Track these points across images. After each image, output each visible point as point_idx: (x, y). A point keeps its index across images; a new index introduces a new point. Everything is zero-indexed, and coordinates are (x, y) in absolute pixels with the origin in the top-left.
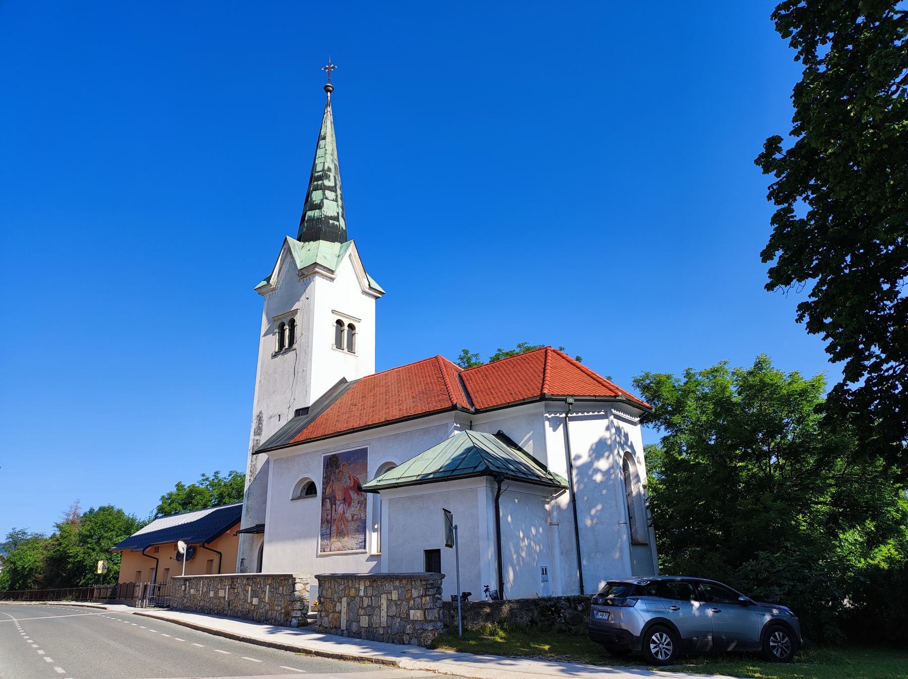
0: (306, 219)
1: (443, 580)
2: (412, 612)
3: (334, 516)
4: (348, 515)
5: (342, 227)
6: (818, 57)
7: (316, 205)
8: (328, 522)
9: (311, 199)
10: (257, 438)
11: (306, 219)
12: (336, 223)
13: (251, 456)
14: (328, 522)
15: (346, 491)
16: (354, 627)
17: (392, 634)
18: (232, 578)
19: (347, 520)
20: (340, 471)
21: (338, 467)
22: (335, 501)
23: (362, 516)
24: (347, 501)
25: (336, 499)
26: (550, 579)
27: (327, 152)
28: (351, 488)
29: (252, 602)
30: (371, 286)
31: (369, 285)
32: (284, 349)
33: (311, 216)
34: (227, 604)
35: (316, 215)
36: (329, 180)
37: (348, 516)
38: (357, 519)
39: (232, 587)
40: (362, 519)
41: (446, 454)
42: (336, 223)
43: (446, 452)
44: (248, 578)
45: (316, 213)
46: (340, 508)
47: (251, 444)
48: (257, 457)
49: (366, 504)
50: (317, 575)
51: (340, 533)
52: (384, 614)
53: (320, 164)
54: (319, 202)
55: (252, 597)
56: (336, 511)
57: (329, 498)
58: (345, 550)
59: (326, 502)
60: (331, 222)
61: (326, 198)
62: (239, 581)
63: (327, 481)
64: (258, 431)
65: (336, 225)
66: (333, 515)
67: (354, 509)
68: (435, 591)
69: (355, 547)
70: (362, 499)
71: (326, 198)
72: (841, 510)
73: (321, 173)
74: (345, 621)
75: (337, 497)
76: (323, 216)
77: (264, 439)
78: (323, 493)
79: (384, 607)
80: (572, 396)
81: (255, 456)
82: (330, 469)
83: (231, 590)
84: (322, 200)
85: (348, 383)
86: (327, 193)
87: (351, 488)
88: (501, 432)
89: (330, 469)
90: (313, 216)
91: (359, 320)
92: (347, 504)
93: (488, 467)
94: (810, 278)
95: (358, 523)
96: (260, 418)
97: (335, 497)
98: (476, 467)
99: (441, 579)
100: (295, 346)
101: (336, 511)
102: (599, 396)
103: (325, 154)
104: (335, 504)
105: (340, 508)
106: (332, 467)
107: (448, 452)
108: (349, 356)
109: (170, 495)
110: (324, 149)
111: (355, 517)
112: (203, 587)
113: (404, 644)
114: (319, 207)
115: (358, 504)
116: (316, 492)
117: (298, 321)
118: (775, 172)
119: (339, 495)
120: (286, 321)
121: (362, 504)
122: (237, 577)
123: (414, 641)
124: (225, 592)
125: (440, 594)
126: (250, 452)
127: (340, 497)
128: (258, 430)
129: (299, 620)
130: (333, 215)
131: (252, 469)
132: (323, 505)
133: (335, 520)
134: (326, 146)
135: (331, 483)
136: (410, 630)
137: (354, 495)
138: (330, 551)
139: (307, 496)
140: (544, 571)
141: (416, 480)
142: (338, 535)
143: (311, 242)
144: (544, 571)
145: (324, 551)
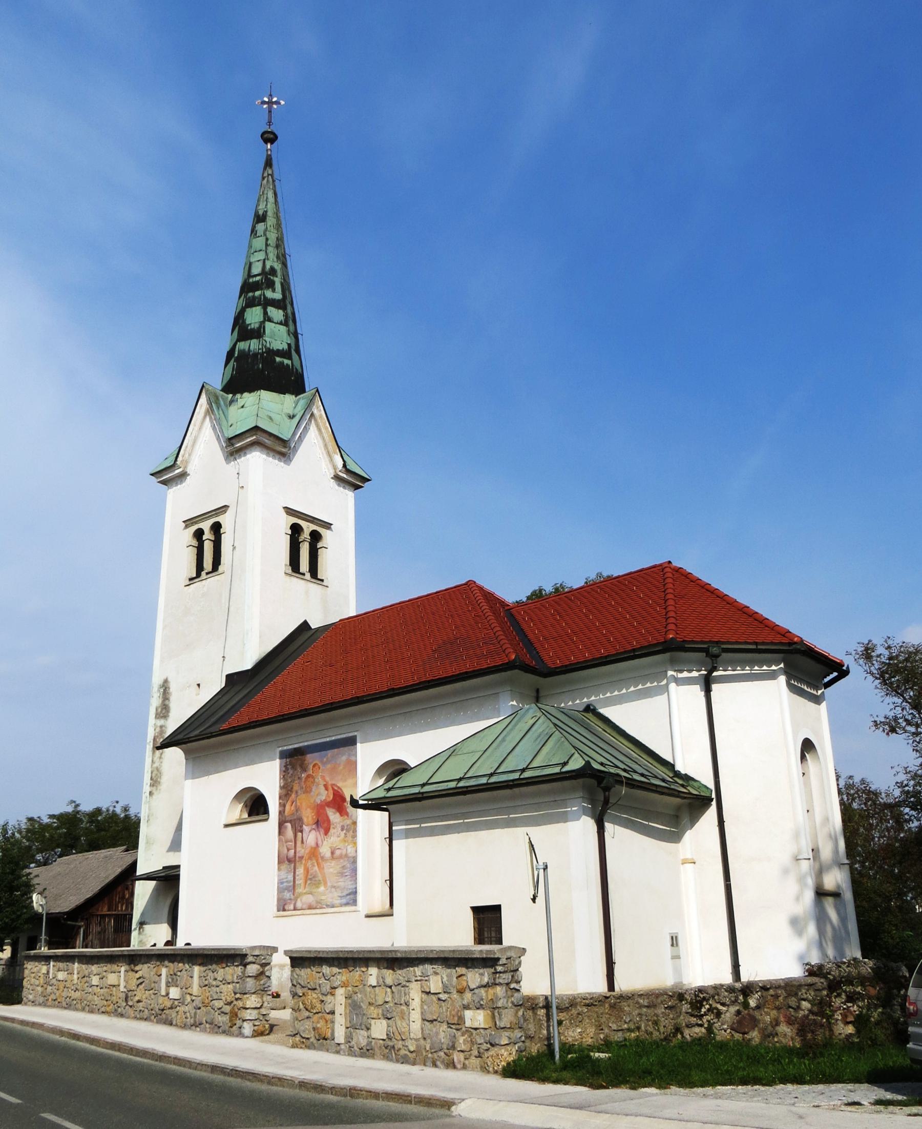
0: (236, 355)
1: (522, 958)
2: (468, 1014)
3: (301, 851)
4: (325, 850)
5: (296, 369)
7: (253, 330)
8: (289, 861)
9: (244, 321)
10: (161, 722)
11: (236, 355)
12: (286, 361)
13: (151, 753)
14: (289, 861)
15: (320, 809)
16: (361, 1038)
17: (433, 1051)
19: (322, 858)
20: (308, 776)
21: (304, 770)
22: (301, 827)
23: (349, 850)
24: (323, 825)
25: (303, 823)
26: (682, 953)
27: (269, 242)
28: (329, 804)
30: (348, 467)
31: (345, 466)
32: (203, 573)
33: (244, 350)
35: (252, 348)
36: (274, 291)
37: (325, 850)
38: (341, 857)
40: (350, 855)
41: (505, 743)
42: (286, 361)
43: (503, 740)
45: (253, 345)
46: (311, 837)
47: (151, 733)
48: (161, 754)
49: (355, 831)
50: (288, 951)
51: (311, 879)
52: (416, 1016)
53: (257, 263)
54: (257, 326)
55: (168, 985)
56: (302, 842)
57: (290, 822)
58: (321, 908)
59: (286, 827)
60: (278, 359)
61: (270, 320)
63: (286, 792)
64: (164, 711)
65: (287, 364)
66: (298, 849)
67: (334, 839)
68: (510, 977)
69: (337, 902)
70: (349, 822)
71: (270, 320)
73: (258, 278)
75: (305, 820)
76: (264, 350)
77: (172, 724)
78: (280, 812)
79: (416, 1003)
80: (717, 642)
81: (158, 752)
82: (291, 771)
84: (262, 324)
85: (311, 633)
86: (272, 311)
87: (329, 804)
88: (592, 707)
89: (291, 771)
90: (247, 350)
91: (328, 526)
92: (322, 831)
93: (588, 763)
95: (343, 862)
96: (165, 687)
97: (300, 820)
98: (565, 764)
99: (520, 957)
100: (221, 568)
101: (302, 842)
102: (763, 643)
103: (267, 245)
104: (301, 831)
105: (311, 837)
106: (294, 768)
107: (508, 739)
108: (314, 587)
110: (263, 239)
111: (338, 853)
113: (455, 1067)
114: (258, 333)
115: (342, 830)
116: (266, 811)
117: (227, 528)
118: (125, 847)
119: (308, 816)
120: (206, 526)
121: (348, 830)
123: (474, 1061)
125: (518, 982)
126: (150, 747)
127: (310, 819)
128: (162, 709)
129: (255, 1026)
130: (281, 348)
131: (154, 775)
132: (280, 833)
133: (301, 858)
134: (268, 233)
135: (293, 796)
136: (465, 1044)
137: (333, 816)
138: (295, 909)
139: (253, 818)
140: (674, 941)
141: (456, 788)
142: (309, 882)
143: (246, 394)
144: (674, 941)
145: (284, 910)
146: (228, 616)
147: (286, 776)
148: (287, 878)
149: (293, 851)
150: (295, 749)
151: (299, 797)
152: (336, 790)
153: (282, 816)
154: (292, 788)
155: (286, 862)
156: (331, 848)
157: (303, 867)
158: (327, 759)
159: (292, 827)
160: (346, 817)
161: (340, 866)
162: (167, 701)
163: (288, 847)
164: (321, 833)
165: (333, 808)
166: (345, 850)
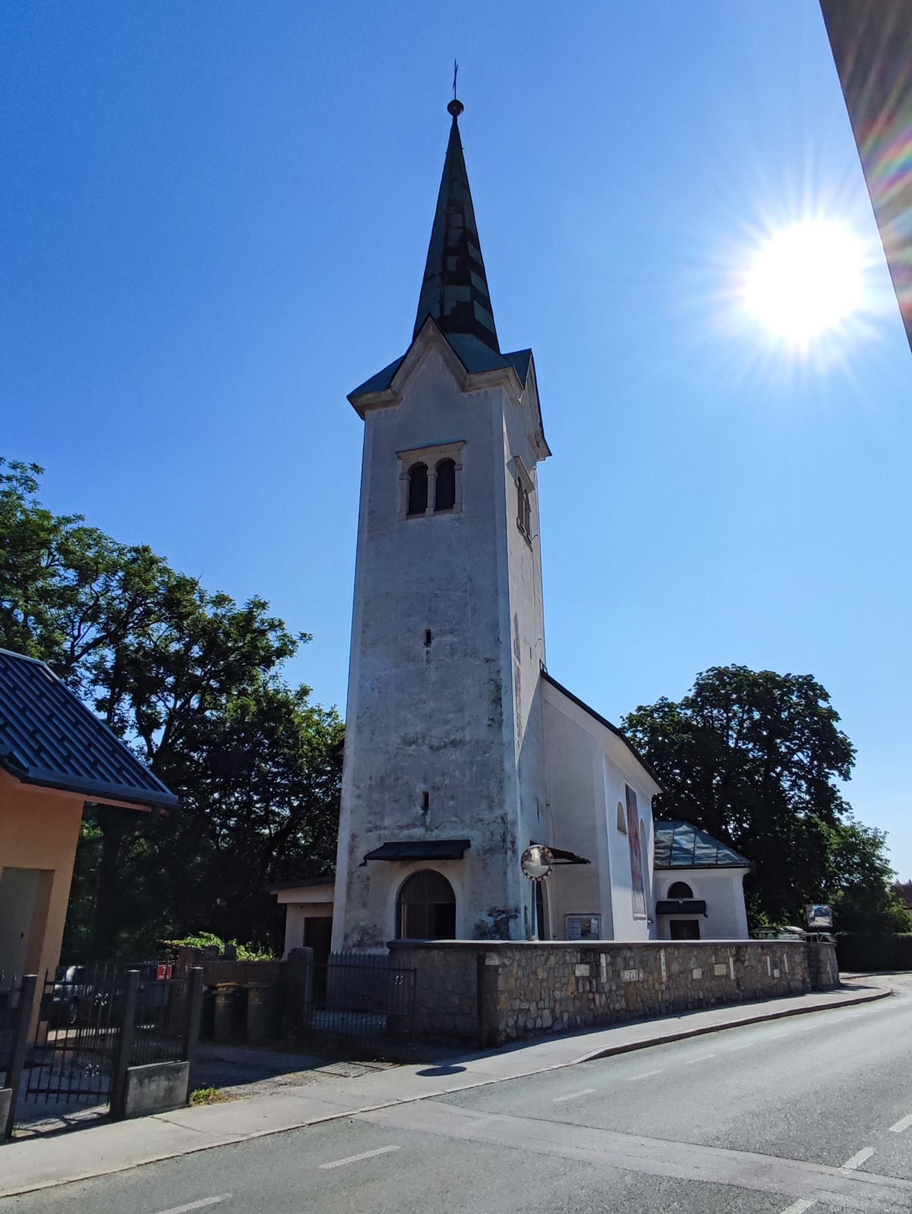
6: (846, 776)
18: (739, 946)
29: (773, 975)
34: (735, 985)
39: (738, 959)
44: (763, 946)
55: (772, 970)
62: (749, 950)
72: (322, 868)
74: (371, 1152)
83: (738, 964)
94: (476, 318)
109: (665, 708)
112: (223, 987)
122: (746, 945)
124: (728, 967)
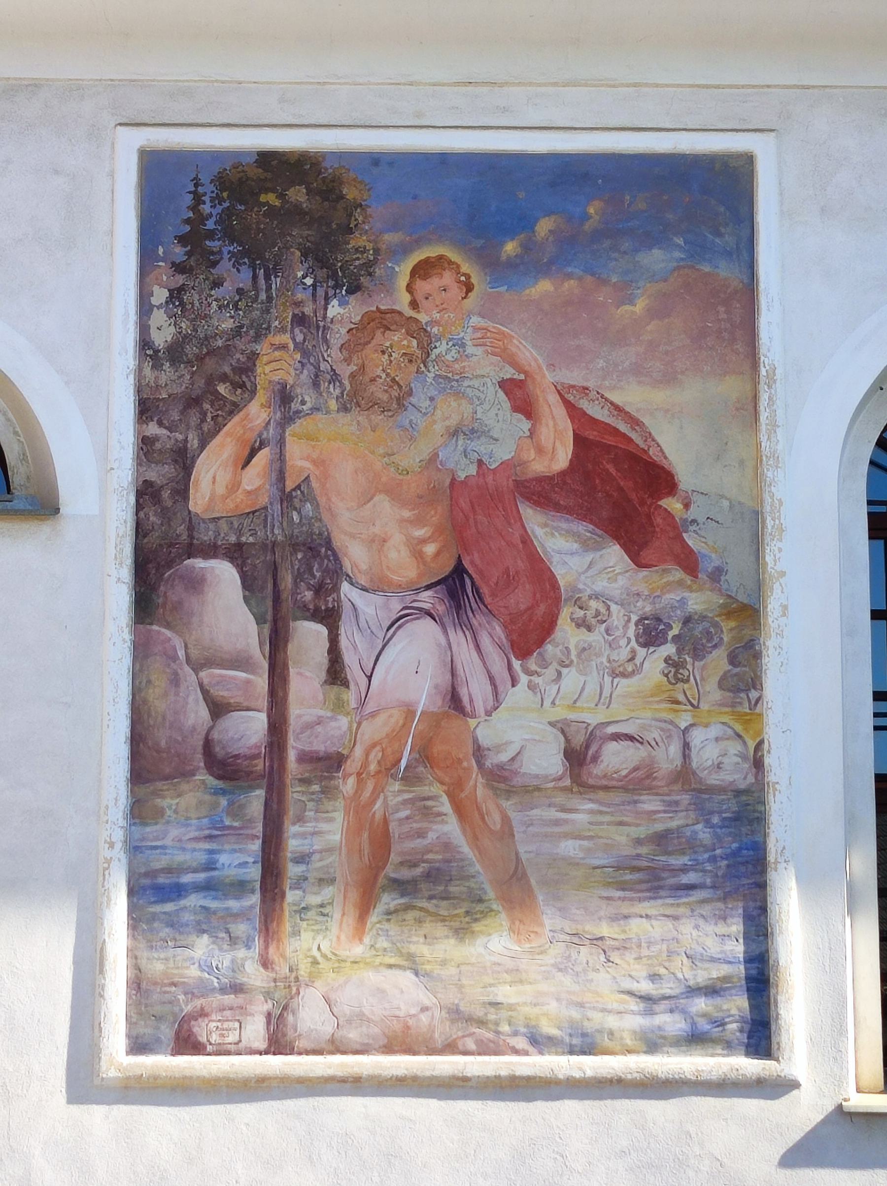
146: (375, 664)
147: (192, 297)
148: (210, 866)
149: (261, 719)
150: (266, 158)
151: (297, 427)
152: (594, 422)
153: (166, 515)
154: (248, 367)
155: (203, 776)
156: (563, 727)
157: (339, 816)
158: (527, 247)
159: (248, 583)
160: (678, 574)
161: (642, 832)
162: (754, 972)
163: (220, 693)
164: (486, 641)
165: (584, 513)
166: (675, 749)
